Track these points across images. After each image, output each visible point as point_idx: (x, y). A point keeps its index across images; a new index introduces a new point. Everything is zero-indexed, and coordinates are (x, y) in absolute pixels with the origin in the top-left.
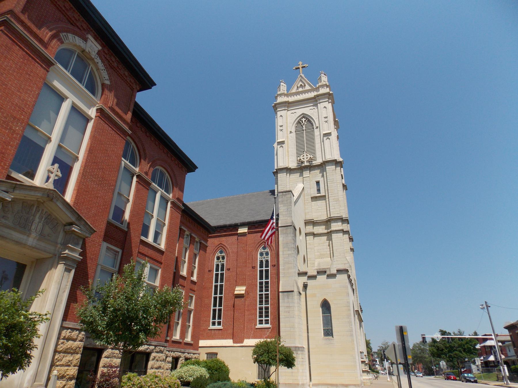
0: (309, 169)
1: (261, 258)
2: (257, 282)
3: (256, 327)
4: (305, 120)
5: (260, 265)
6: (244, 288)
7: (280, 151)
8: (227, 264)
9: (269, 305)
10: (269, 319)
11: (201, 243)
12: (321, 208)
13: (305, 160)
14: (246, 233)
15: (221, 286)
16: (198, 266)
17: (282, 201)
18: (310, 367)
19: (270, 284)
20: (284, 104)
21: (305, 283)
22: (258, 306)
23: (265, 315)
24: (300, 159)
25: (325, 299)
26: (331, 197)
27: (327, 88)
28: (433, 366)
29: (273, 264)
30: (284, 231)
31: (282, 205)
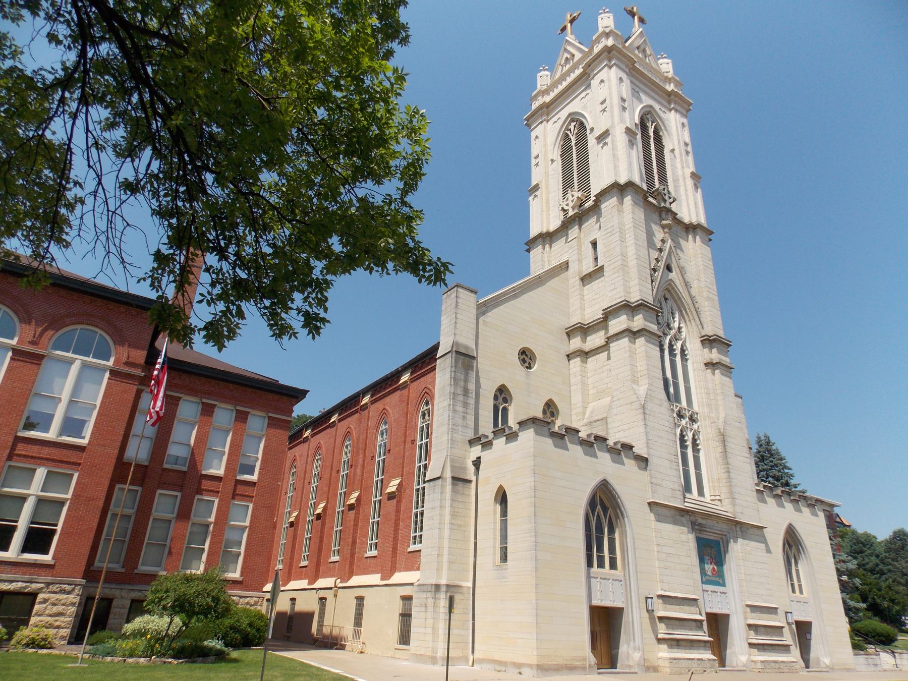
0: (577, 222)
7: (535, 205)
12: (597, 296)
16: (263, 457)
18: (473, 624)
25: (605, 480)
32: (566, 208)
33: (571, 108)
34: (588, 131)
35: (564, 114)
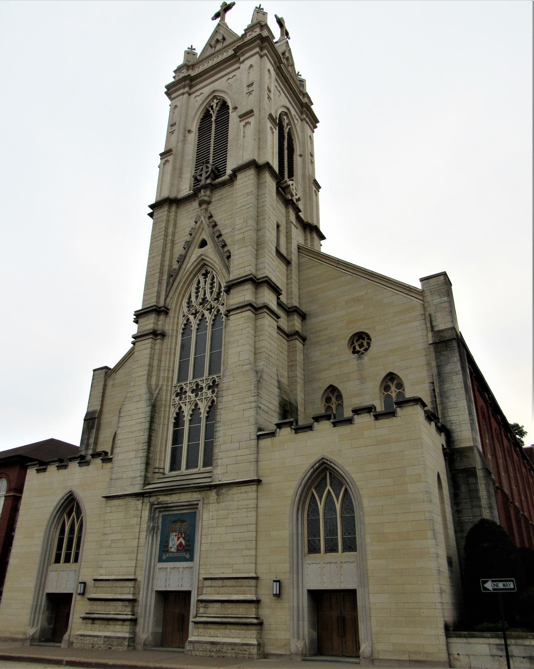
32: (199, 178)
33: (216, 86)
34: (230, 110)
35: (207, 91)
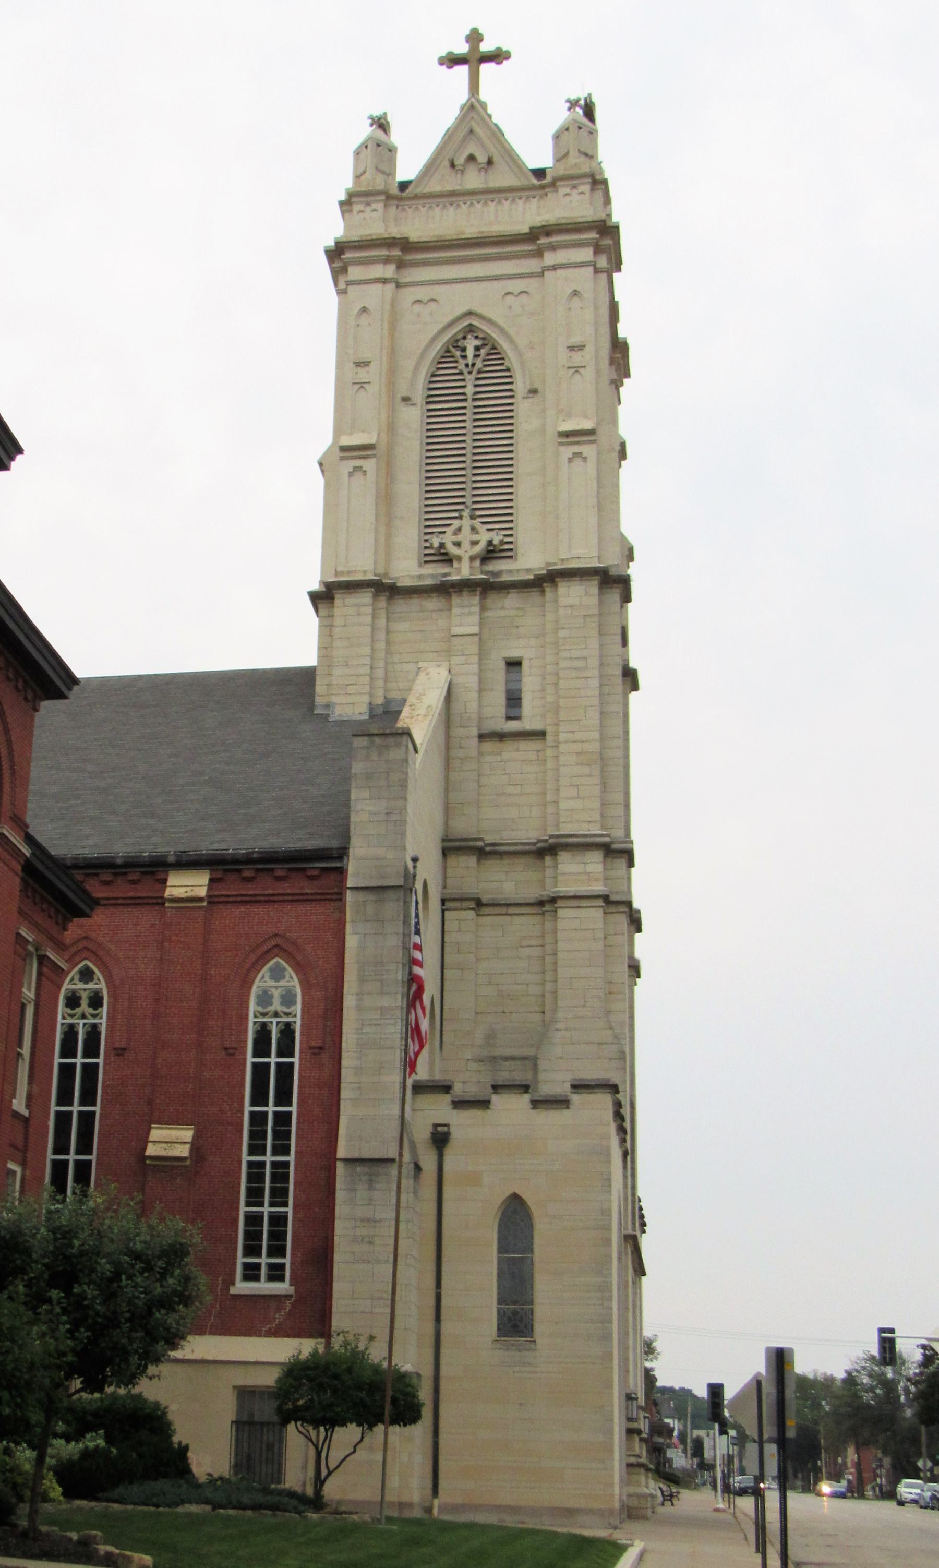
1: (264, 1015)
2: (242, 1112)
3: (233, 1291)
4: (477, 348)
5: (256, 1042)
6: (187, 1134)
8: (110, 1028)
9: (289, 1210)
10: (287, 1261)
11: (42, 959)
12: (518, 790)
13: (466, 552)
14: (200, 899)
15: (87, 1120)
17: (368, 776)
19: (298, 1123)
20: (384, 252)
21: (439, 1129)
22: (243, 1209)
23: (269, 1247)
24: (442, 545)
26: (566, 742)
27: (592, 190)
28: (919, 1455)
29: (313, 1044)
30: (370, 909)
31: (366, 794)
